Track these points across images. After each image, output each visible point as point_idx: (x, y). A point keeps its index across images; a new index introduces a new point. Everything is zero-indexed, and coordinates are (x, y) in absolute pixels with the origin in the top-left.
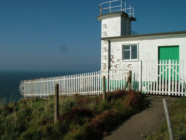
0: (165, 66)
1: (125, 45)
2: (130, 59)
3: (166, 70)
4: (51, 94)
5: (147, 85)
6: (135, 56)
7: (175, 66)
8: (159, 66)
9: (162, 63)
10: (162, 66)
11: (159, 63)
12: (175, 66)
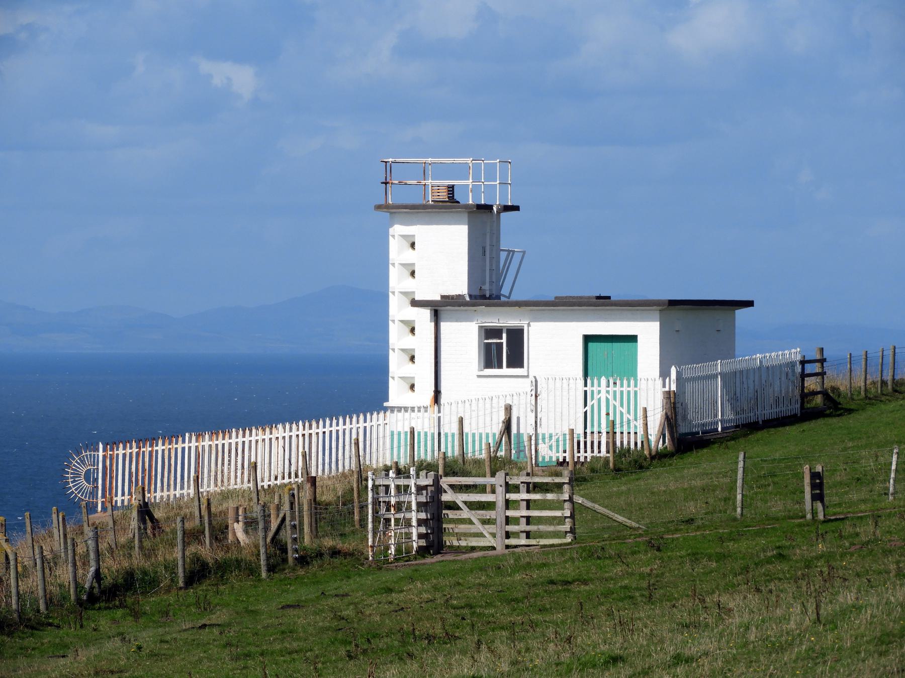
0: (592, 392)
3: (595, 402)
4: (231, 487)
7: (615, 392)
8: (586, 392)
9: (593, 385)
10: (629, 392)
11: (586, 385)
12: (615, 392)
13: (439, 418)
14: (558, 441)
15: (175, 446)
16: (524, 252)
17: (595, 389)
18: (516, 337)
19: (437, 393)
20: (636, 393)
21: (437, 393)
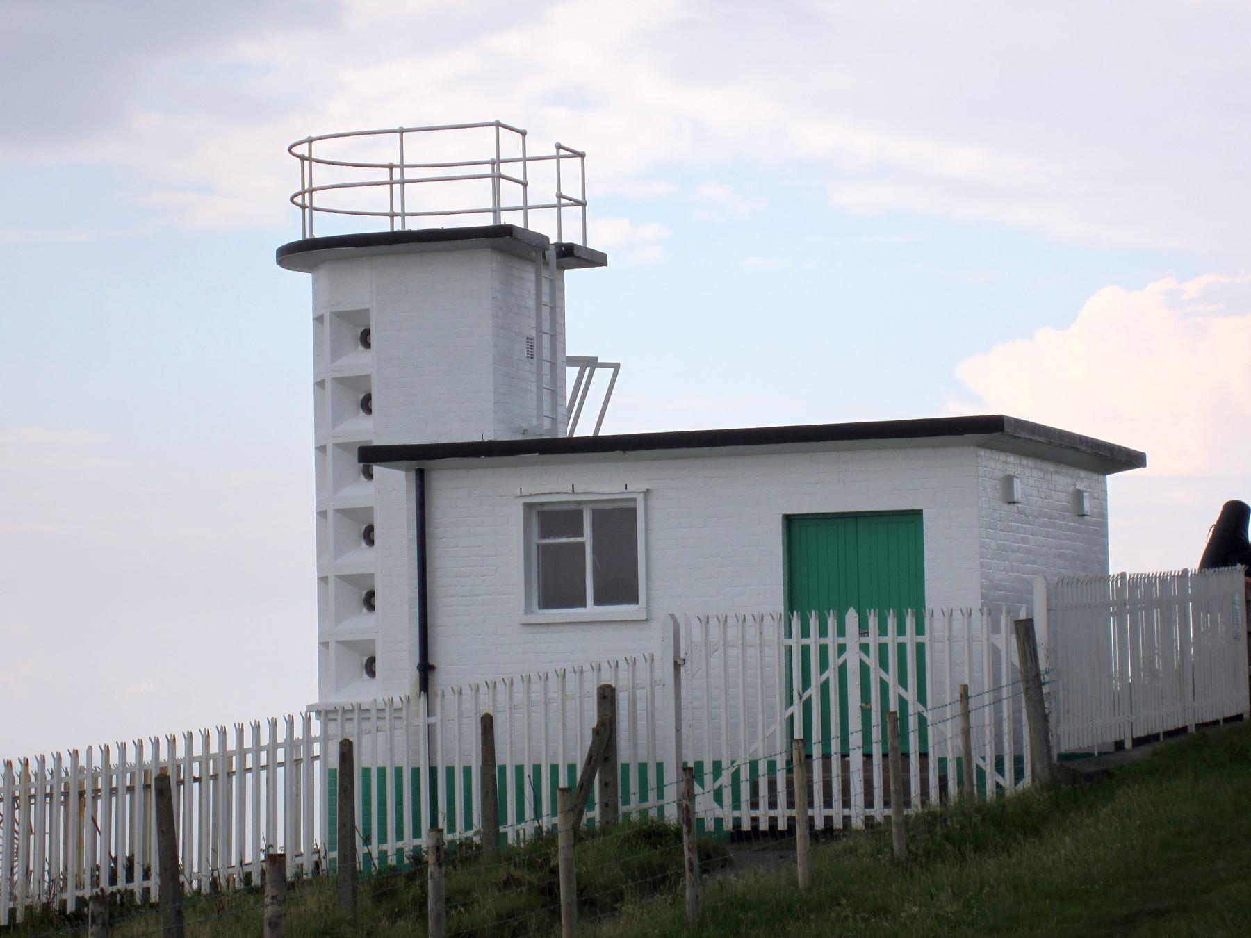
0: (824, 650)
1: (542, 504)
2: (583, 604)
3: (832, 674)
5: (804, 689)
6: (619, 585)
7: (883, 648)
12: (883, 648)
13: (431, 729)
14: (736, 776)
15: (794, 813)
16: (616, 366)
17: (831, 641)
18: (618, 524)
19: (426, 669)
20: (920, 648)
21: (426, 669)
